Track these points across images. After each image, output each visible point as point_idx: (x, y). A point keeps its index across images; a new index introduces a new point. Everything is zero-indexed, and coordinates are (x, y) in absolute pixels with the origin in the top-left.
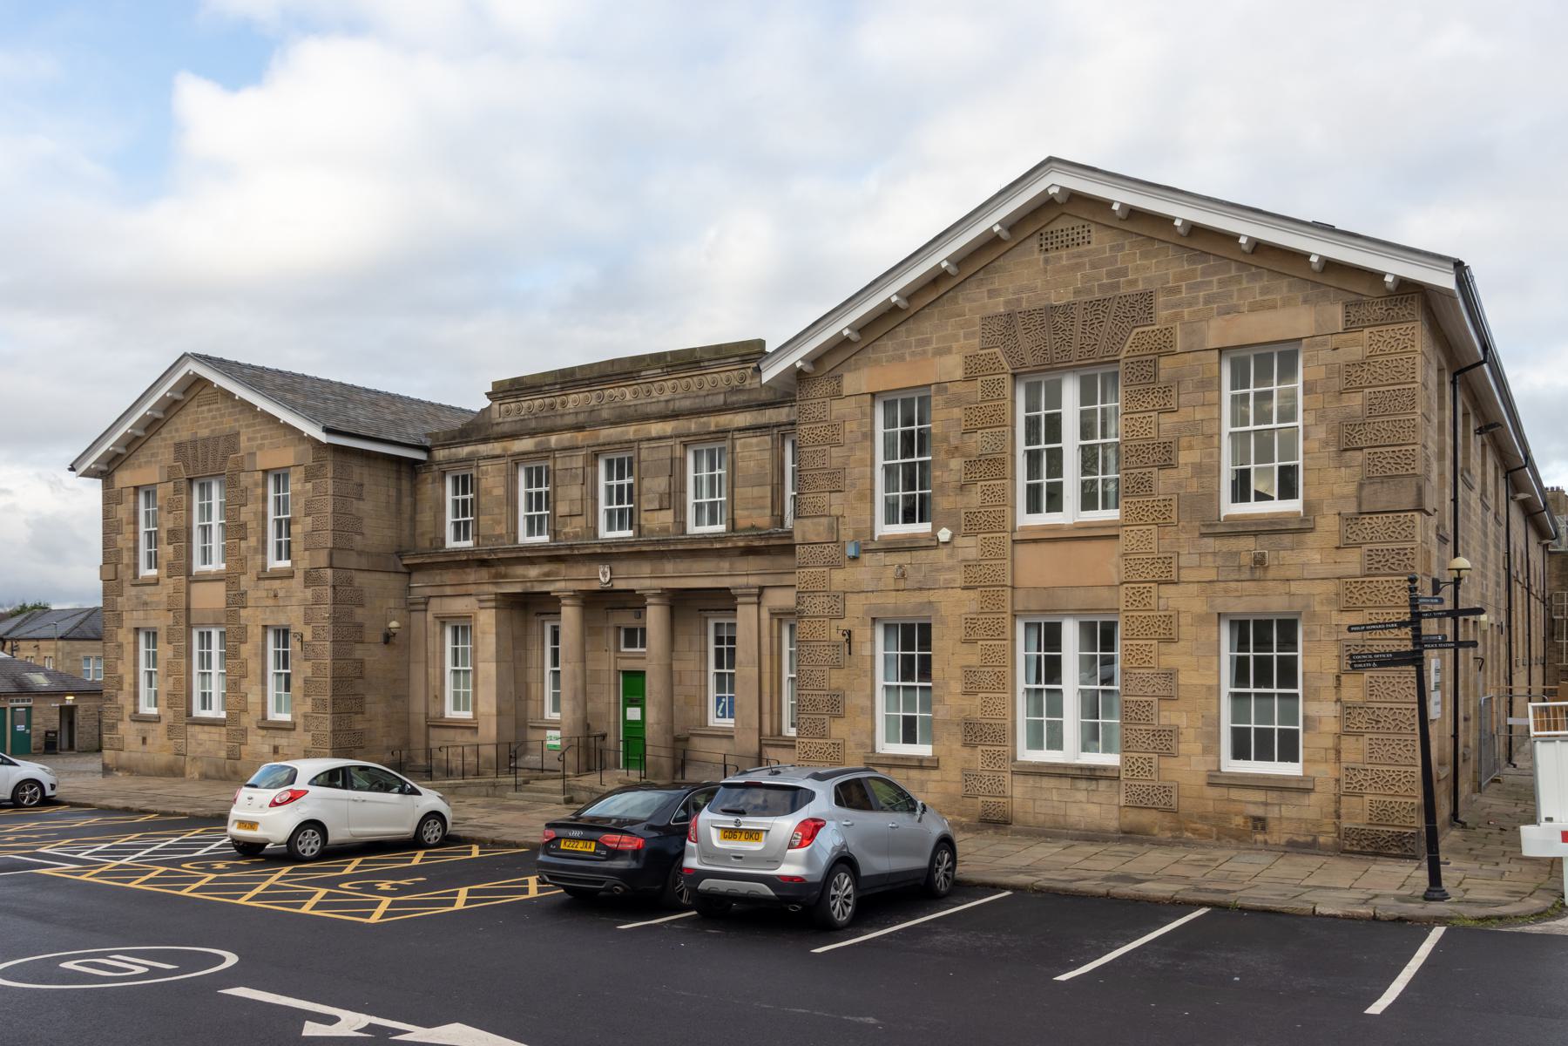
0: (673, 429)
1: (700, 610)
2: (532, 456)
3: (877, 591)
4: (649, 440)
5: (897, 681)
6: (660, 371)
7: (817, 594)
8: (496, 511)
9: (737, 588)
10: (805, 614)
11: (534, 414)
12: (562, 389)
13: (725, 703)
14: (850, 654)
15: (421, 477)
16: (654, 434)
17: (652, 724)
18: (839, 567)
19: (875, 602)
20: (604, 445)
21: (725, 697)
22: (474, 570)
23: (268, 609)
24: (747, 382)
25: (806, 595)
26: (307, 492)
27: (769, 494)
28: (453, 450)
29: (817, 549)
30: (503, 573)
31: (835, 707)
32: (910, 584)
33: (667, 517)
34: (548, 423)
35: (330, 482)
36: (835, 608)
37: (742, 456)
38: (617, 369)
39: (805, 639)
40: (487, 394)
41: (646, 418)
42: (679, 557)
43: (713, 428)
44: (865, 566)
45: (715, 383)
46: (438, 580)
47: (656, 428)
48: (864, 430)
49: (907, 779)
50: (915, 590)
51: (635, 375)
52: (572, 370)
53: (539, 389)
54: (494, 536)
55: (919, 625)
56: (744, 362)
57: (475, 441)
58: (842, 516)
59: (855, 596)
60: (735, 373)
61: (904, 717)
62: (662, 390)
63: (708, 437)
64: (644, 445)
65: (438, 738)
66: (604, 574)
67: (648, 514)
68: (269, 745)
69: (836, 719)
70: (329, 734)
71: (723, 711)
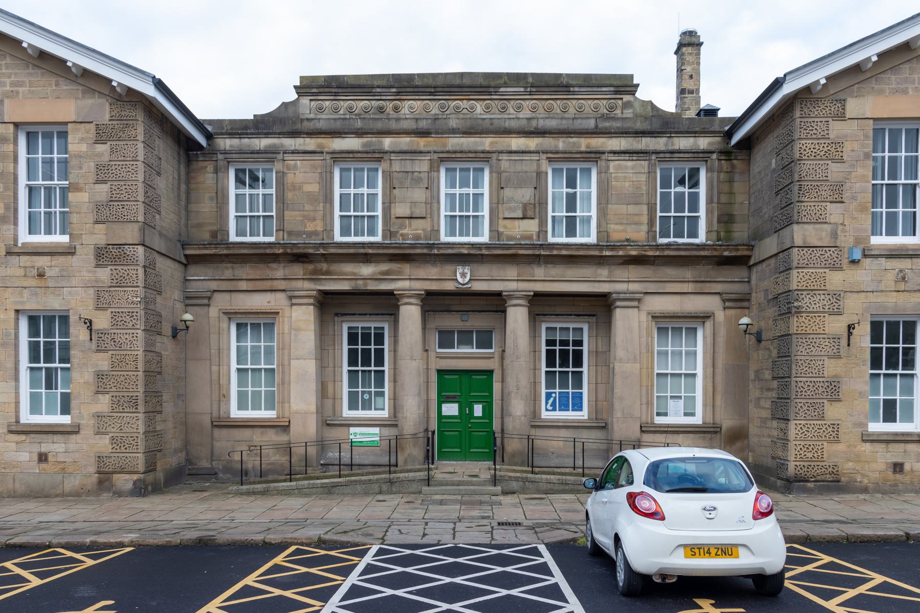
0: (537, 145)
1: (538, 315)
2: (359, 155)
3: (876, 291)
4: (511, 152)
6: (522, 89)
7: (817, 292)
8: (308, 207)
10: (804, 310)
11: (356, 115)
12: (398, 93)
13: (555, 398)
14: (849, 345)
15: (195, 165)
16: (514, 148)
17: (519, 416)
18: (841, 269)
19: (874, 301)
20: (455, 152)
21: (555, 393)
22: (282, 265)
23: (26, 291)
24: (618, 112)
25: (805, 293)
26: (100, 155)
28: (246, 140)
29: (819, 252)
30: (324, 269)
31: (835, 392)
32: (909, 286)
33: (531, 226)
34: (379, 125)
35: (141, 146)
36: (836, 305)
37: (616, 177)
38: (466, 81)
39: (803, 332)
40: (295, 87)
41: (508, 132)
42: (552, 263)
43: (583, 149)
45: (580, 110)
46: (228, 274)
47: (516, 143)
48: (866, 150)
49: (905, 452)
51: (492, 90)
52: (410, 77)
53: (369, 90)
54: (304, 233)
55: (887, 322)
56: (616, 92)
57: (279, 134)
58: (842, 224)
59: (855, 295)
60: (605, 102)
61: (896, 400)
62: (519, 108)
63: (578, 156)
64: (504, 157)
65: (224, 440)
66: (463, 275)
68: (30, 452)
69: (833, 403)
70: (141, 436)
71: (553, 404)
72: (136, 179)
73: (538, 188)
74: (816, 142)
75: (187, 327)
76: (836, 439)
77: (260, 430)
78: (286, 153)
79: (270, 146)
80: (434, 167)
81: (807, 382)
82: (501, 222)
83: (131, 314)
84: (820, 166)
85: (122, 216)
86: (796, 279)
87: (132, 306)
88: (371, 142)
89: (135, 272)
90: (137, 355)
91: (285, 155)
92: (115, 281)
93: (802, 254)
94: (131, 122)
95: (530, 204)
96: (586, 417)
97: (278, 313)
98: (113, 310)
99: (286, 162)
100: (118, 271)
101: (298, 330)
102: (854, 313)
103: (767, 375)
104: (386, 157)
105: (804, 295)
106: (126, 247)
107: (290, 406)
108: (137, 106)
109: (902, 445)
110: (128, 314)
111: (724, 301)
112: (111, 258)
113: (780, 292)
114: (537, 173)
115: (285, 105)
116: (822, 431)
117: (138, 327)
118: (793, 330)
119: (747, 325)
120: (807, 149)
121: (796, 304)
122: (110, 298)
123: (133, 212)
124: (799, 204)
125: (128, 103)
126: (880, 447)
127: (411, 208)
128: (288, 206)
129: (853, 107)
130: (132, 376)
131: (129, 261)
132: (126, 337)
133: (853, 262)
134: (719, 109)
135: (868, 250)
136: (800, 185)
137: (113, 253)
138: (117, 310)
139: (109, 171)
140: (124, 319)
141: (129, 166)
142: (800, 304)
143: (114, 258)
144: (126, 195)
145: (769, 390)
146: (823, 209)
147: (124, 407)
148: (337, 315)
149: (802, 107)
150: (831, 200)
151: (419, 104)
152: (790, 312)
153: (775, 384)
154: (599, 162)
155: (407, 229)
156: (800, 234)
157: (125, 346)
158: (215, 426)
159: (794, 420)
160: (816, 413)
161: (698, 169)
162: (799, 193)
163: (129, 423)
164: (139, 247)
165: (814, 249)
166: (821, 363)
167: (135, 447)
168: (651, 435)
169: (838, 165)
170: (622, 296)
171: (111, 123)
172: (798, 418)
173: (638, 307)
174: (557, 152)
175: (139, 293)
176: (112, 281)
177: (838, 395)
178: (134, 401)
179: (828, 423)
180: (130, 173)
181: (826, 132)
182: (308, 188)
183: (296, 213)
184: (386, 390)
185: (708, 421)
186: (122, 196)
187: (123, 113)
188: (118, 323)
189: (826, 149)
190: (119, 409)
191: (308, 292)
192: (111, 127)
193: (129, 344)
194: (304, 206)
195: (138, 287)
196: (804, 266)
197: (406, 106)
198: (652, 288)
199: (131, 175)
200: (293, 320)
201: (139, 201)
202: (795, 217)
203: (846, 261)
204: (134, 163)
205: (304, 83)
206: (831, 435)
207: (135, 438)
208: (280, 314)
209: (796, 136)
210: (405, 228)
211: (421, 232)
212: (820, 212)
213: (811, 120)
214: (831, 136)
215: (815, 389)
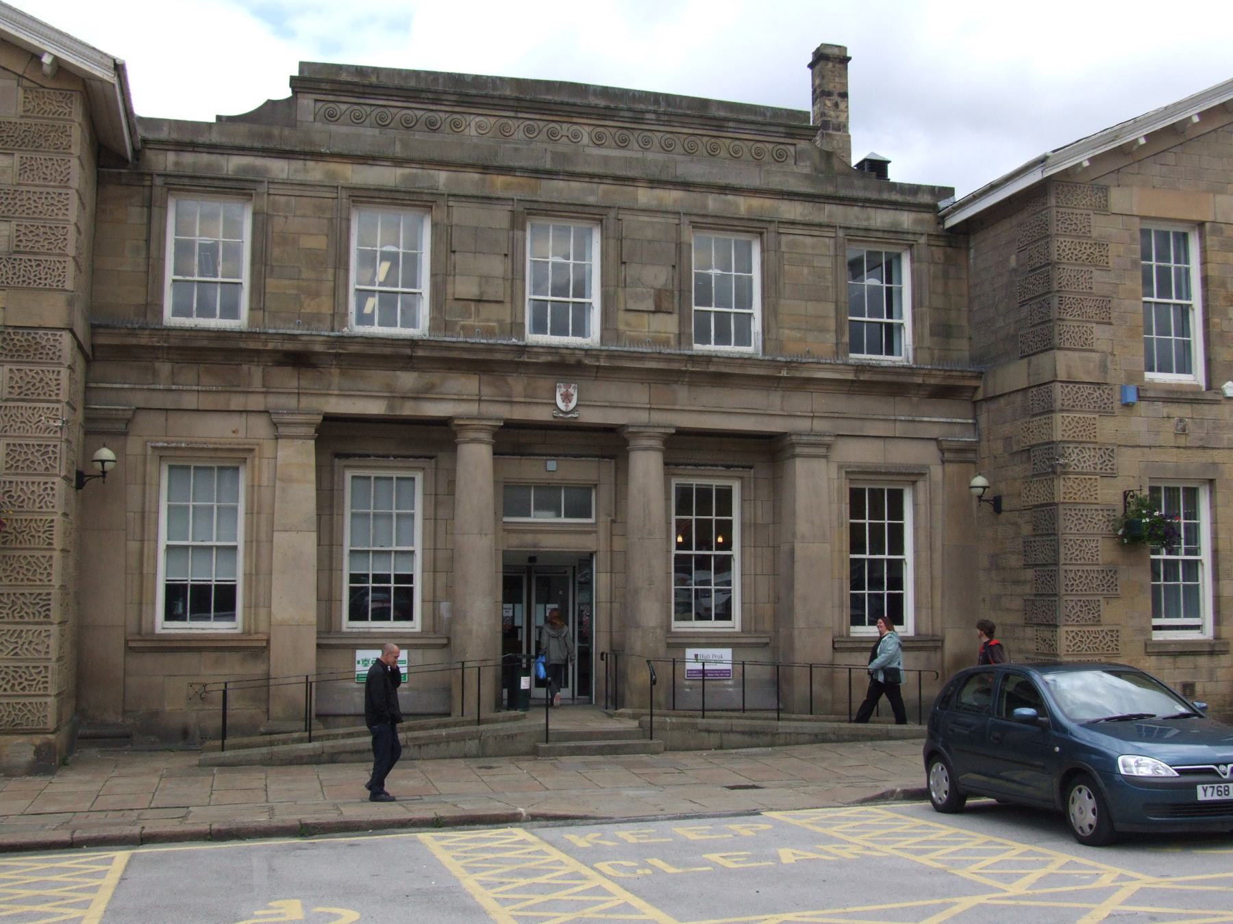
5: (412, 553)
7: (1087, 446)
8: (307, 273)
9: (801, 435)
10: (1071, 469)
17: (653, 628)
18: (1112, 414)
27: (832, 314)
33: (667, 325)
39: (1072, 501)
44: (1140, 416)
47: (645, 196)
49: (1195, 668)
50: (1198, 448)
59: (1129, 451)
60: (770, 146)
66: (567, 398)
67: (631, 317)
72: (65, 218)
73: (677, 268)
74: (1076, 241)
75: (104, 473)
76: (1116, 652)
77: (209, 657)
78: (272, 182)
79: (245, 170)
80: (517, 222)
81: (1078, 571)
82: (622, 315)
83: (43, 449)
84: (1082, 273)
85: (36, 278)
86: (1061, 427)
87: (46, 435)
88: (415, 175)
89: (55, 376)
90: (52, 521)
91: (271, 186)
92: (17, 391)
93: (1066, 392)
94: (61, 123)
95: (666, 291)
96: (738, 628)
97: (251, 450)
98: (11, 441)
99: (272, 197)
100: (23, 374)
101: (288, 480)
102: (1129, 476)
103: (1014, 561)
104: (441, 202)
105: (1071, 450)
106: (41, 332)
107: (270, 614)
108: (73, 99)
109: (1191, 658)
110: (37, 448)
111: (942, 451)
112: (11, 350)
113: (1034, 442)
114: (676, 244)
115: (271, 104)
116: (1098, 640)
117: (57, 471)
118: (1059, 497)
119: (984, 488)
120: (1067, 250)
121: (1061, 461)
122: (6, 419)
123: (56, 273)
124: (1061, 323)
125: (58, 92)
126: (1167, 661)
127: (480, 285)
128: (272, 271)
129: (1119, 199)
130: (41, 559)
131: (44, 356)
132: (32, 489)
133: (1128, 405)
134: (889, 162)
135: (1143, 390)
136: (1060, 297)
137: (15, 341)
138: (17, 441)
139: (17, 201)
140: (30, 456)
141: (53, 195)
142: (1066, 461)
143: (17, 351)
144: (46, 243)
145: (1017, 582)
146: (1089, 332)
147: (22, 614)
148: (338, 456)
149: (1058, 193)
150: (1098, 320)
151: (492, 122)
152: (1054, 472)
153: (1029, 574)
154: (765, 234)
155: (473, 319)
156: (1066, 362)
157: (30, 505)
158: (130, 648)
159: (1066, 625)
160: (1091, 616)
161: (899, 256)
162: (1059, 308)
163: (31, 642)
164: (63, 333)
165: (1081, 386)
166: (1094, 545)
167: (41, 686)
168: (846, 655)
169: (1103, 273)
170: (805, 439)
171: (23, 121)
172: (1069, 623)
173: (825, 457)
174: (704, 216)
175: (59, 413)
176: (10, 390)
177: (1116, 590)
178: (42, 603)
179: (1106, 628)
180: (55, 208)
181: (1087, 229)
182: (308, 242)
183: (286, 282)
184: (346, 585)
185: (923, 630)
186: (38, 245)
187: (47, 108)
188: (20, 464)
189: (1088, 251)
190: (14, 617)
191: (308, 417)
192: (23, 128)
193: (37, 501)
194: (300, 272)
195: (58, 401)
196: (1070, 408)
197: (473, 124)
198: (844, 427)
199: (56, 211)
200: (278, 463)
201: (68, 256)
202: (1057, 341)
203: (1117, 404)
204: (64, 191)
205: (306, 74)
206: (1109, 646)
207: (41, 668)
208: (256, 452)
209: (1053, 230)
210: (470, 318)
211: (495, 324)
212: (1086, 336)
213: (1070, 211)
214: (1094, 234)
215: (1088, 581)
